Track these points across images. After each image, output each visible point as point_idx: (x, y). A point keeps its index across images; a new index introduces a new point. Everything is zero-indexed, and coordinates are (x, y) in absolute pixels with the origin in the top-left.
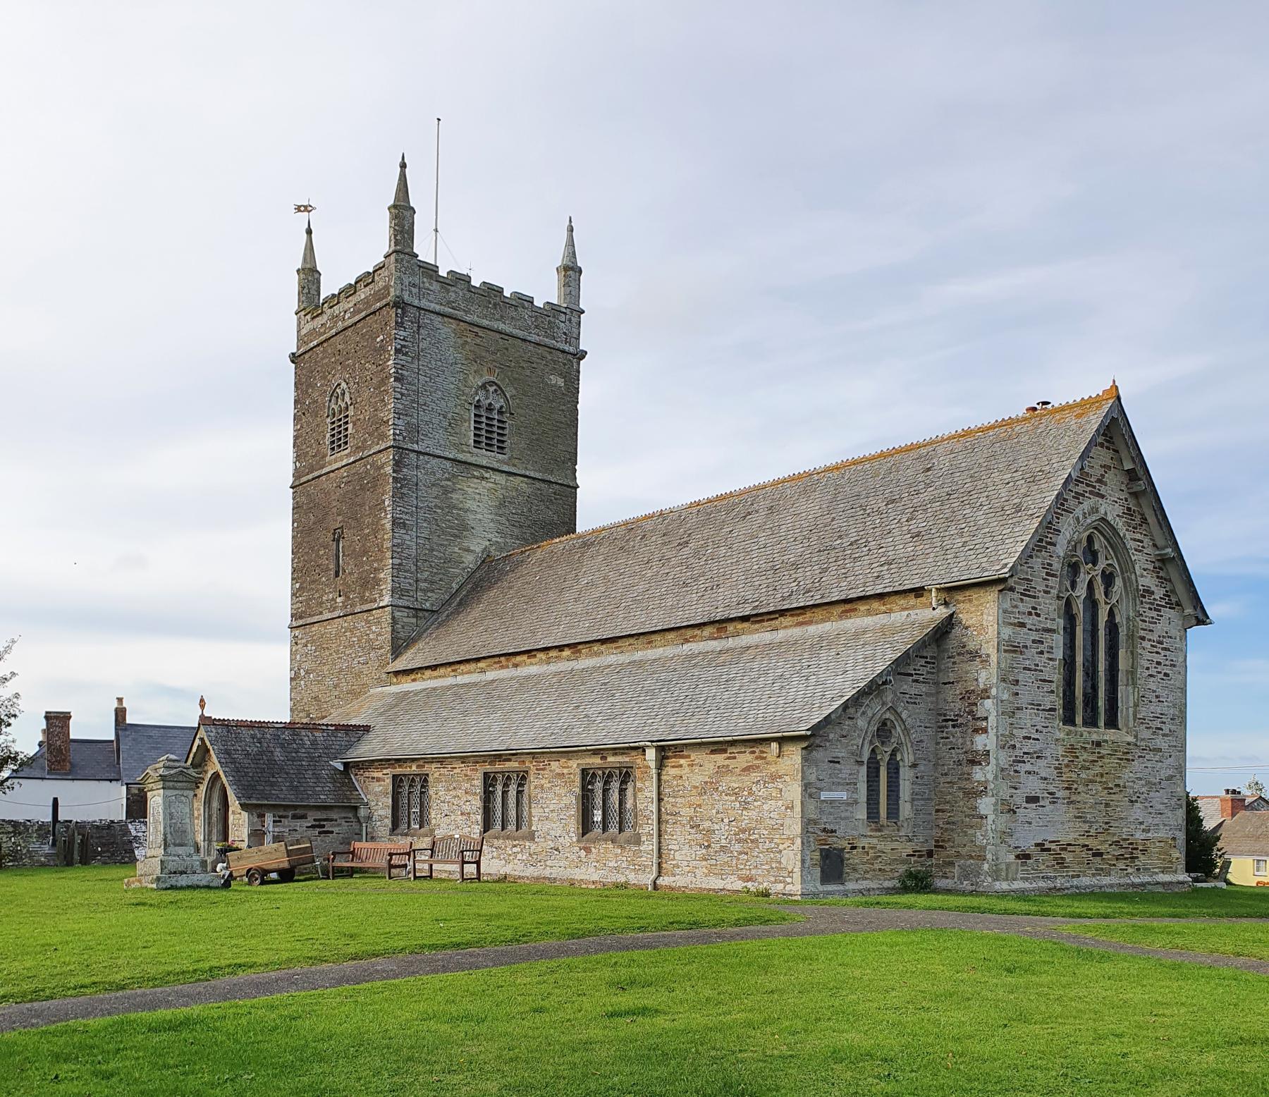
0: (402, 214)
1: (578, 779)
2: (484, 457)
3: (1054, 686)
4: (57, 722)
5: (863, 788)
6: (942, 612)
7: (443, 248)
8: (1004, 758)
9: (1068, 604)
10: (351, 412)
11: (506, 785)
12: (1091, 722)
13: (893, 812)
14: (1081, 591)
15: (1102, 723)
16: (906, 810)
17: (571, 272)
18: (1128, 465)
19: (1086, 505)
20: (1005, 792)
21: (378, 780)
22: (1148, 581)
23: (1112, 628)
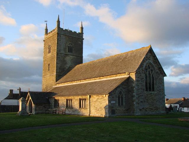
0: (59, 22)
1: (79, 100)
2: (68, 53)
3: (144, 86)
4: (11, 91)
5: (117, 101)
6: (128, 76)
7: (63, 26)
8: (137, 96)
9: (146, 74)
10: (51, 48)
11: (69, 101)
12: (150, 90)
13: (122, 104)
14: (148, 73)
15: (148, 90)
16: (124, 104)
17: (82, 28)
18: (153, 55)
19: (148, 61)
20: (137, 101)
21: (53, 100)
22: (158, 71)
23: (153, 78)
